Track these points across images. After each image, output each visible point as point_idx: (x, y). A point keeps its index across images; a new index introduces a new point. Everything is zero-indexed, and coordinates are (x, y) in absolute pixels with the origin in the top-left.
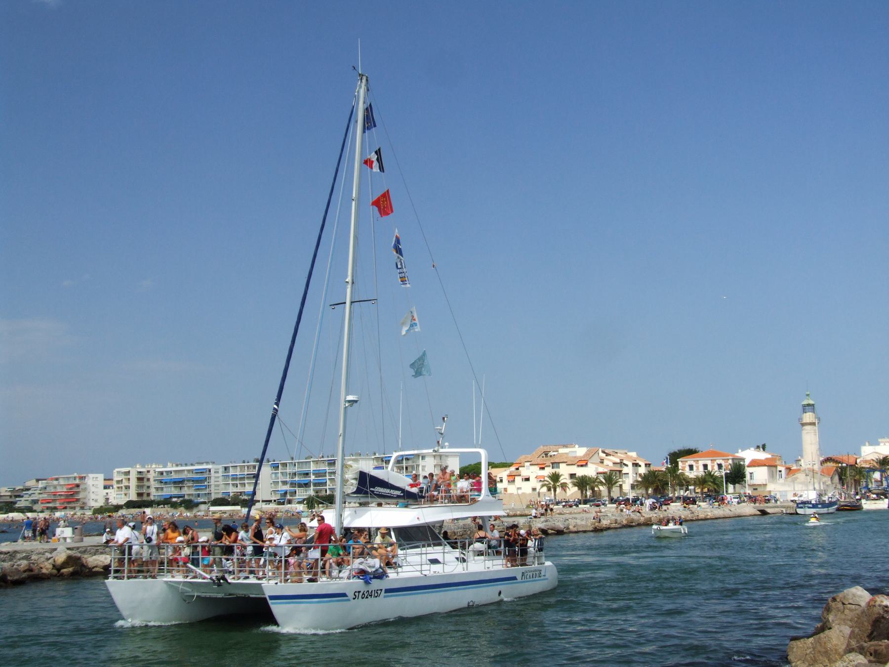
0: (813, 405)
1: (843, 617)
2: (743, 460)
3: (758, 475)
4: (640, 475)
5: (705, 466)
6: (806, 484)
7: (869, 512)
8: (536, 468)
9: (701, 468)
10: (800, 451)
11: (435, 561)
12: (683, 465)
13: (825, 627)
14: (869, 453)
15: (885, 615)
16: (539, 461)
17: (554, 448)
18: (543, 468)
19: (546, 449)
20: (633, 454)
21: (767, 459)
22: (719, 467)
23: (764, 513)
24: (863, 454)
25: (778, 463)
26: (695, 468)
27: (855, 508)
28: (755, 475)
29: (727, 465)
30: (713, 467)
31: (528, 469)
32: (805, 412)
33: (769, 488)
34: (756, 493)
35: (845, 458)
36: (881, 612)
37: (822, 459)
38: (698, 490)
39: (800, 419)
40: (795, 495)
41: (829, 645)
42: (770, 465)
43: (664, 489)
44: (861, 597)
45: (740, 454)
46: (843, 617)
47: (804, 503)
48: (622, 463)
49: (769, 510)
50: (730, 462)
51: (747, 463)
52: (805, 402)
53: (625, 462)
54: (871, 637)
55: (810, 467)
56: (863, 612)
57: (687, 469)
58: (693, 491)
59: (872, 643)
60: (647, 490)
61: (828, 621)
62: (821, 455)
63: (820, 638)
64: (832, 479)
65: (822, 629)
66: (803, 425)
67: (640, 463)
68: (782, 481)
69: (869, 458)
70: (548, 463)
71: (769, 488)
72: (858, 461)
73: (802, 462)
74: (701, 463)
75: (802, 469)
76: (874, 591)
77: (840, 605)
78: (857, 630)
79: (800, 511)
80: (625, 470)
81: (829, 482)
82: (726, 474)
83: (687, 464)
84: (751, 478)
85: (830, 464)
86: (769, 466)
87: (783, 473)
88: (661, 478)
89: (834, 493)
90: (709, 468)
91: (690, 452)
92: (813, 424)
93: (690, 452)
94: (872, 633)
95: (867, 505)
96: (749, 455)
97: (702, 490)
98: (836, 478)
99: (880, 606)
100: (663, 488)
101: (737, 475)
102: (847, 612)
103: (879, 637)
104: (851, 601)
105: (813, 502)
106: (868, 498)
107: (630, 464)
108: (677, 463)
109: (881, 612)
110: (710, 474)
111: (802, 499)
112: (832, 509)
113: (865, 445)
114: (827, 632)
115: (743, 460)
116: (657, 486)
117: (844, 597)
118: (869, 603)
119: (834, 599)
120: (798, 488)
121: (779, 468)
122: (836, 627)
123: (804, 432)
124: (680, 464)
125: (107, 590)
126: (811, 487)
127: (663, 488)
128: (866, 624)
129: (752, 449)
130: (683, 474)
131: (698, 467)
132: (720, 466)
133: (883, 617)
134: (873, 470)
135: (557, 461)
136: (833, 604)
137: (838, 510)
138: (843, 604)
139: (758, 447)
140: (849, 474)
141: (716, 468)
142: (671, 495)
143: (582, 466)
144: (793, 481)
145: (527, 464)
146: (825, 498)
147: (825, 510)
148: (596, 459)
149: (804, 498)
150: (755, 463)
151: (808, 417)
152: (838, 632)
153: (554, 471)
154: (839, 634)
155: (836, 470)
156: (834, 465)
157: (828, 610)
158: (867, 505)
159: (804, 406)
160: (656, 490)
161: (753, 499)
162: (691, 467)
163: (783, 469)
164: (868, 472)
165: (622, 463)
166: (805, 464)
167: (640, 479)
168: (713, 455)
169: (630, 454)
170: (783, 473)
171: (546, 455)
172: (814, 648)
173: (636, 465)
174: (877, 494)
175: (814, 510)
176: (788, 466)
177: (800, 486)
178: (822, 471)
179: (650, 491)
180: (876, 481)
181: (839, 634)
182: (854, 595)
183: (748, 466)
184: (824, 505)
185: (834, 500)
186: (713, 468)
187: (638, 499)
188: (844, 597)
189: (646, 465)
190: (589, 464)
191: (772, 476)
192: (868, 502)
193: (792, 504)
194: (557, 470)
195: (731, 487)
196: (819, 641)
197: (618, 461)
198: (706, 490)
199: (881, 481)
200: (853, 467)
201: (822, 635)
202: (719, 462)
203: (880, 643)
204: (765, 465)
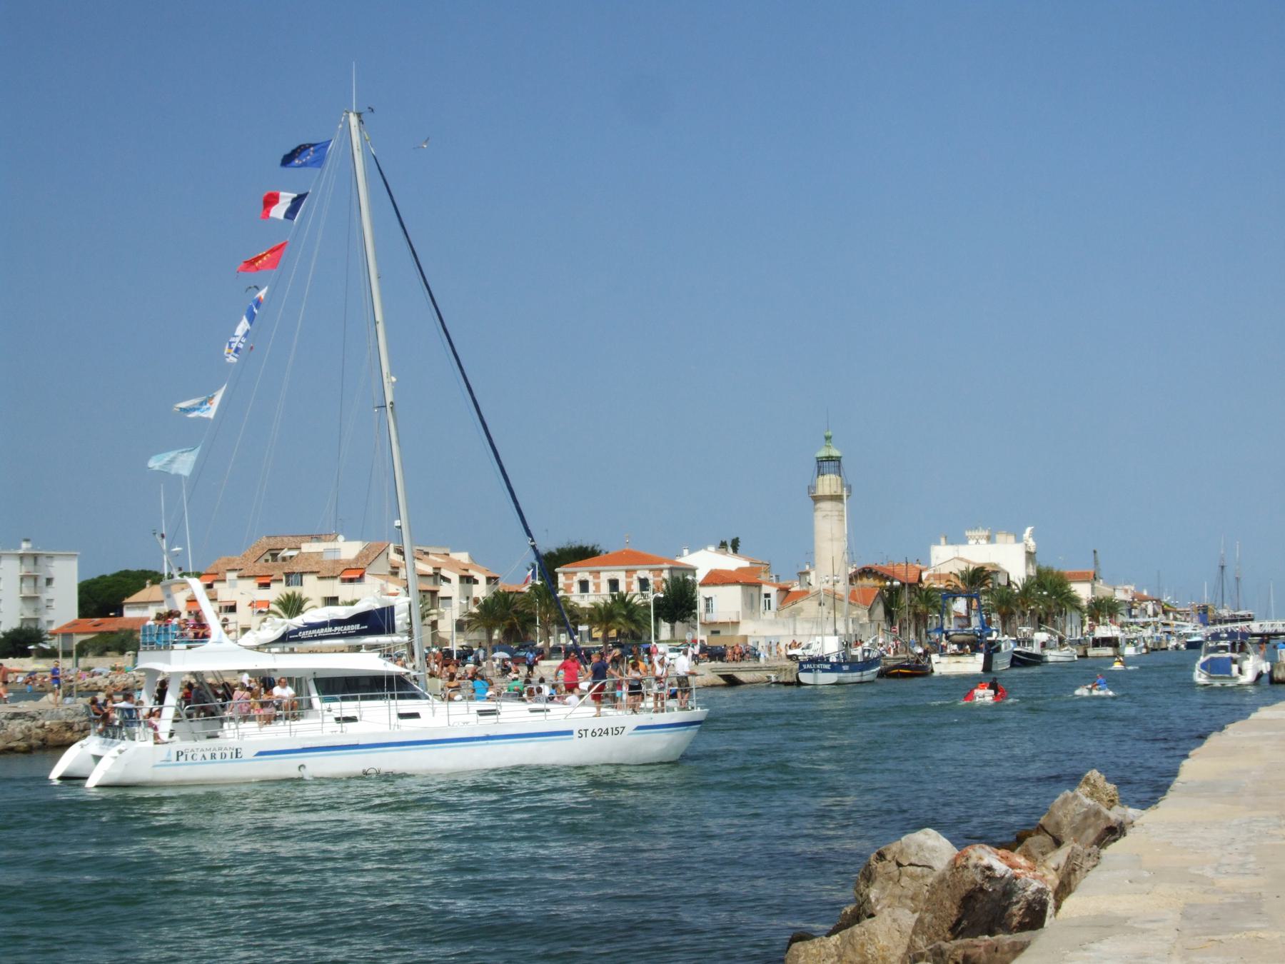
0: (838, 459)
1: (898, 891)
2: (693, 570)
3: (723, 603)
4: (476, 601)
5: (614, 584)
6: (817, 621)
7: (944, 678)
8: (252, 584)
9: (605, 588)
10: (809, 555)
11: (806, 804)
12: (568, 581)
13: (862, 912)
14: (946, 560)
15: (986, 886)
16: (257, 570)
17: (293, 542)
18: (267, 585)
19: (273, 543)
20: (463, 557)
21: (741, 570)
22: (639, 584)
23: (731, 681)
24: (934, 562)
25: (763, 577)
26: (591, 587)
27: (919, 670)
28: (716, 604)
29: (659, 580)
30: (629, 585)
31: (233, 586)
32: (820, 473)
33: (744, 630)
34: (717, 642)
35: (900, 570)
36: (979, 878)
37: (851, 571)
38: (599, 634)
39: (812, 488)
40: (795, 645)
41: (871, 950)
42: (748, 581)
43: (526, 631)
44: (933, 849)
45: (687, 559)
46: (898, 891)
47: (816, 663)
48: (437, 576)
49: (742, 676)
50: (666, 575)
51: (700, 577)
52: (823, 453)
53: (444, 572)
54: (956, 931)
55: (829, 586)
56: (942, 880)
57: (576, 588)
58: (590, 636)
59: (959, 942)
60: (490, 634)
61: (868, 899)
62: (851, 562)
63: (852, 935)
64: (871, 611)
65: (856, 918)
66: (817, 499)
67: (477, 576)
68: (770, 615)
69: (945, 570)
70: (278, 574)
71: (744, 630)
72: (924, 575)
73: (812, 578)
74: (605, 577)
75: (812, 591)
76: (963, 839)
77: (893, 868)
78: (928, 917)
79: (805, 677)
80: (444, 590)
81: (865, 619)
82: (657, 600)
83: (576, 579)
84: (708, 608)
85: (869, 582)
86: (746, 585)
87: (773, 599)
88: (520, 609)
89: (879, 641)
90: (622, 588)
91: (581, 554)
92: (837, 498)
93: (581, 554)
94: (958, 922)
95: (943, 666)
96: (704, 561)
97: (606, 632)
98: (880, 611)
99: (976, 866)
100: (524, 628)
101: (679, 602)
102: (905, 881)
103: (973, 931)
104: (914, 860)
105: (833, 659)
106: (942, 651)
107: (455, 578)
108: (555, 576)
109: (979, 878)
110: (621, 601)
111: (810, 652)
112: (870, 674)
113: (938, 543)
114: (867, 922)
115: (693, 570)
116: (512, 626)
117: (902, 851)
118: (955, 860)
119: (881, 856)
120: (803, 631)
121: (766, 589)
122: (886, 911)
123: (819, 515)
124: (562, 579)
125: (949, 839)
126: (830, 630)
127: (524, 628)
128: (948, 904)
129: (712, 549)
130: (567, 599)
131: (597, 586)
132: (644, 583)
133: (982, 890)
134: (953, 594)
135: (298, 569)
136: (880, 865)
137: (881, 674)
138: (899, 865)
139: (723, 545)
140: (902, 600)
141: (636, 587)
142: (539, 644)
143: (351, 580)
144: (794, 615)
145: (231, 576)
146: (857, 652)
147: (854, 677)
148: (382, 566)
149: (814, 652)
150: (717, 579)
151: (828, 484)
152: (889, 920)
153: (290, 590)
154: (892, 925)
155: (881, 594)
156: (877, 583)
157: (869, 877)
158: (943, 666)
159: (820, 461)
160: (510, 634)
161: (713, 654)
162: (584, 586)
163: (772, 591)
164: (945, 598)
165: (437, 576)
166: (818, 580)
167: (475, 610)
168: (630, 559)
169: (455, 556)
170: (773, 599)
171: (274, 556)
172: (840, 957)
173: (468, 580)
174: (961, 645)
175: (833, 677)
176: (783, 583)
177: (808, 626)
178: (853, 596)
179: (496, 635)
180: (958, 617)
181: (892, 925)
182: (920, 847)
183: (702, 584)
184: (855, 665)
185: (874, 654)
186: (629, 586)
187: (471, 652)
188: (902, 851)
189: (489, 580)
190: (367, 578)
191: (750, 604)
192: (944, 660)
193: (789, 664)
194: (296, 589)
195: (665, 628)
196: (850, 942)
197: (430, 571)
198: (613, 633)
199: (968, 618)
200: (915, 587)
201: (857, 929)
202: (643, 574)
203: (976, 941)
204: (737, 583)
